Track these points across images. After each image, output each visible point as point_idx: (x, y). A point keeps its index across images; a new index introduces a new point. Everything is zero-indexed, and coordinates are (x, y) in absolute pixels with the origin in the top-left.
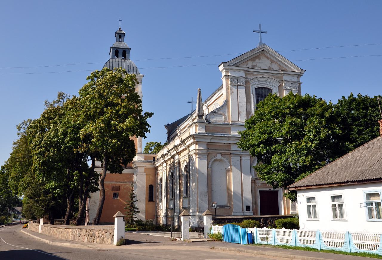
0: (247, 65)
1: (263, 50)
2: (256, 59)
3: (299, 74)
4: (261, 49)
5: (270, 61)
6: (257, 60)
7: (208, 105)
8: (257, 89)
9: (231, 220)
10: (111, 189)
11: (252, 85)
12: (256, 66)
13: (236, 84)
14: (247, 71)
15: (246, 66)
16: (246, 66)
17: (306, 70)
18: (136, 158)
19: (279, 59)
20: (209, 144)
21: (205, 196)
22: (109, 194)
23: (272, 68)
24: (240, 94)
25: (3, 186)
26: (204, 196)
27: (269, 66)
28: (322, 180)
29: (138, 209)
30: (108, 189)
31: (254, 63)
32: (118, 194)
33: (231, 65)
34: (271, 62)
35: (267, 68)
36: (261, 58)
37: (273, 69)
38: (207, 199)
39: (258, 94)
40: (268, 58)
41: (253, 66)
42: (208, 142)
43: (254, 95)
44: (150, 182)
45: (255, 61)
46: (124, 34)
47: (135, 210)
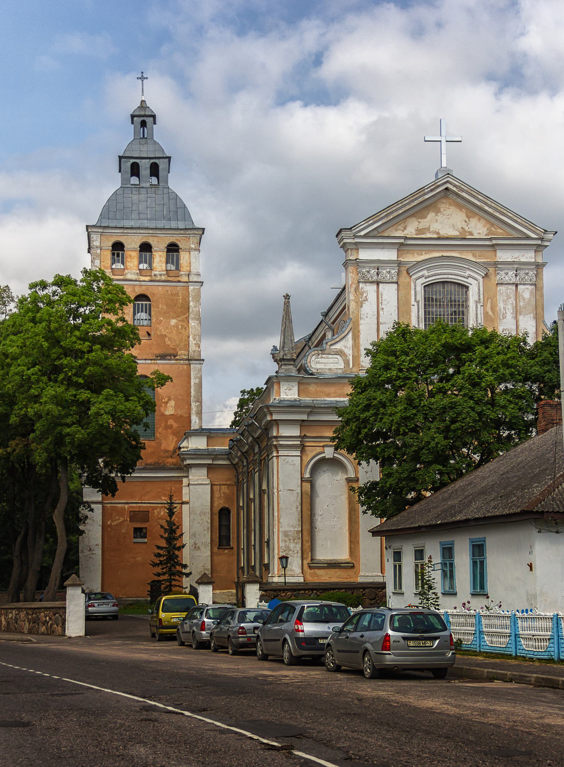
0: (405, 228)
1: (447, 189)
2: (429, 211)
3: (539, 242)
4: (439, 186)
5: (464, 215)
6: (431, 215)
7: (324, 324)
8: (427, 287)
9: (301, 592)
10: (129, 519)
11: (417, 279)
12: (428, 229)
13: (375, 278)
14: (402, 244)
15: (403, 231)
16: (403, 231)
17: (556, 232)
18: (60, 475)
19: (486, 208)
20: (305, 424)
21: (294, 540)
22: (124, 531)
23: (471, 233)
24: (384, 302)
25: (476, 392)
26: (292, 541)
27: (462, 228)
28: (299, 520)
29: (185, 566)
30: (122, 519)
31: (424, 223)
32: (144, 531)
33: (362, 233)
34: (468, 217)
35: (455, 233)
36: (442, 210)
37: (472, 234)
38: (299, 546)
39: (432, 299)
40: (460, 207)
41: (419, 231)
42: (303, 421)
43: (418, 305)
44: (221, 502)
45: (426, 217)
46: (7, 286)
47: (178, 568)
